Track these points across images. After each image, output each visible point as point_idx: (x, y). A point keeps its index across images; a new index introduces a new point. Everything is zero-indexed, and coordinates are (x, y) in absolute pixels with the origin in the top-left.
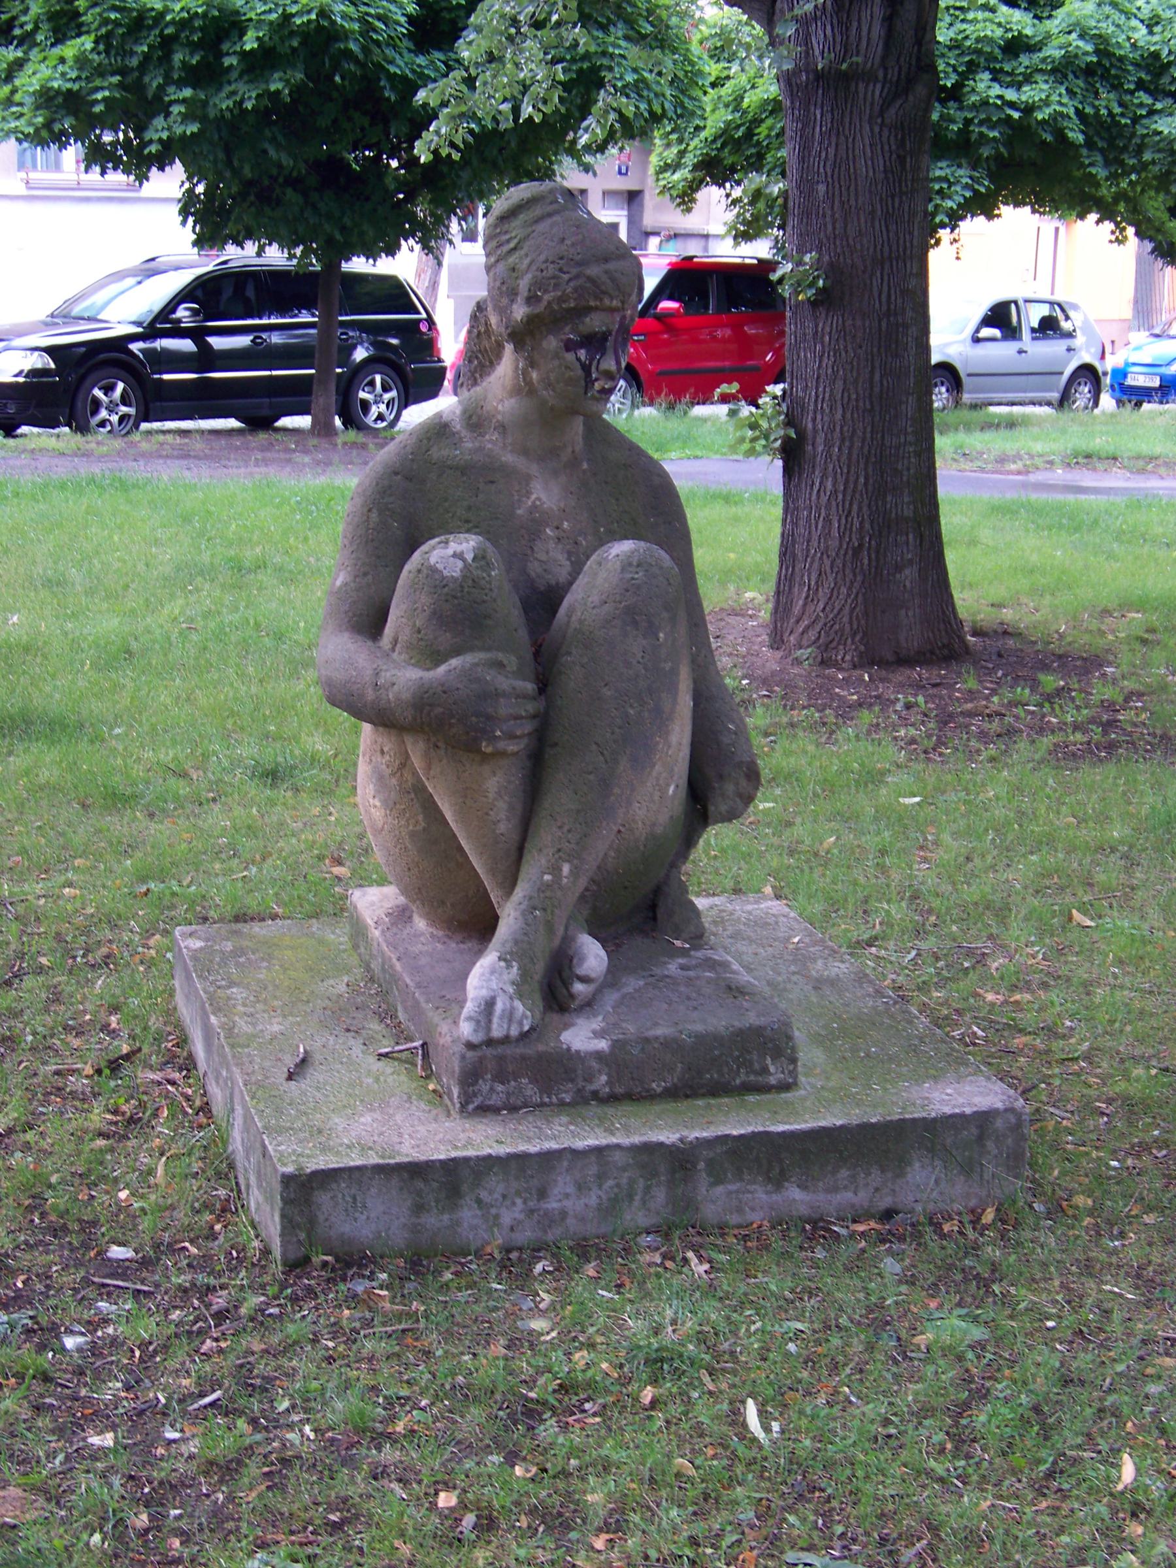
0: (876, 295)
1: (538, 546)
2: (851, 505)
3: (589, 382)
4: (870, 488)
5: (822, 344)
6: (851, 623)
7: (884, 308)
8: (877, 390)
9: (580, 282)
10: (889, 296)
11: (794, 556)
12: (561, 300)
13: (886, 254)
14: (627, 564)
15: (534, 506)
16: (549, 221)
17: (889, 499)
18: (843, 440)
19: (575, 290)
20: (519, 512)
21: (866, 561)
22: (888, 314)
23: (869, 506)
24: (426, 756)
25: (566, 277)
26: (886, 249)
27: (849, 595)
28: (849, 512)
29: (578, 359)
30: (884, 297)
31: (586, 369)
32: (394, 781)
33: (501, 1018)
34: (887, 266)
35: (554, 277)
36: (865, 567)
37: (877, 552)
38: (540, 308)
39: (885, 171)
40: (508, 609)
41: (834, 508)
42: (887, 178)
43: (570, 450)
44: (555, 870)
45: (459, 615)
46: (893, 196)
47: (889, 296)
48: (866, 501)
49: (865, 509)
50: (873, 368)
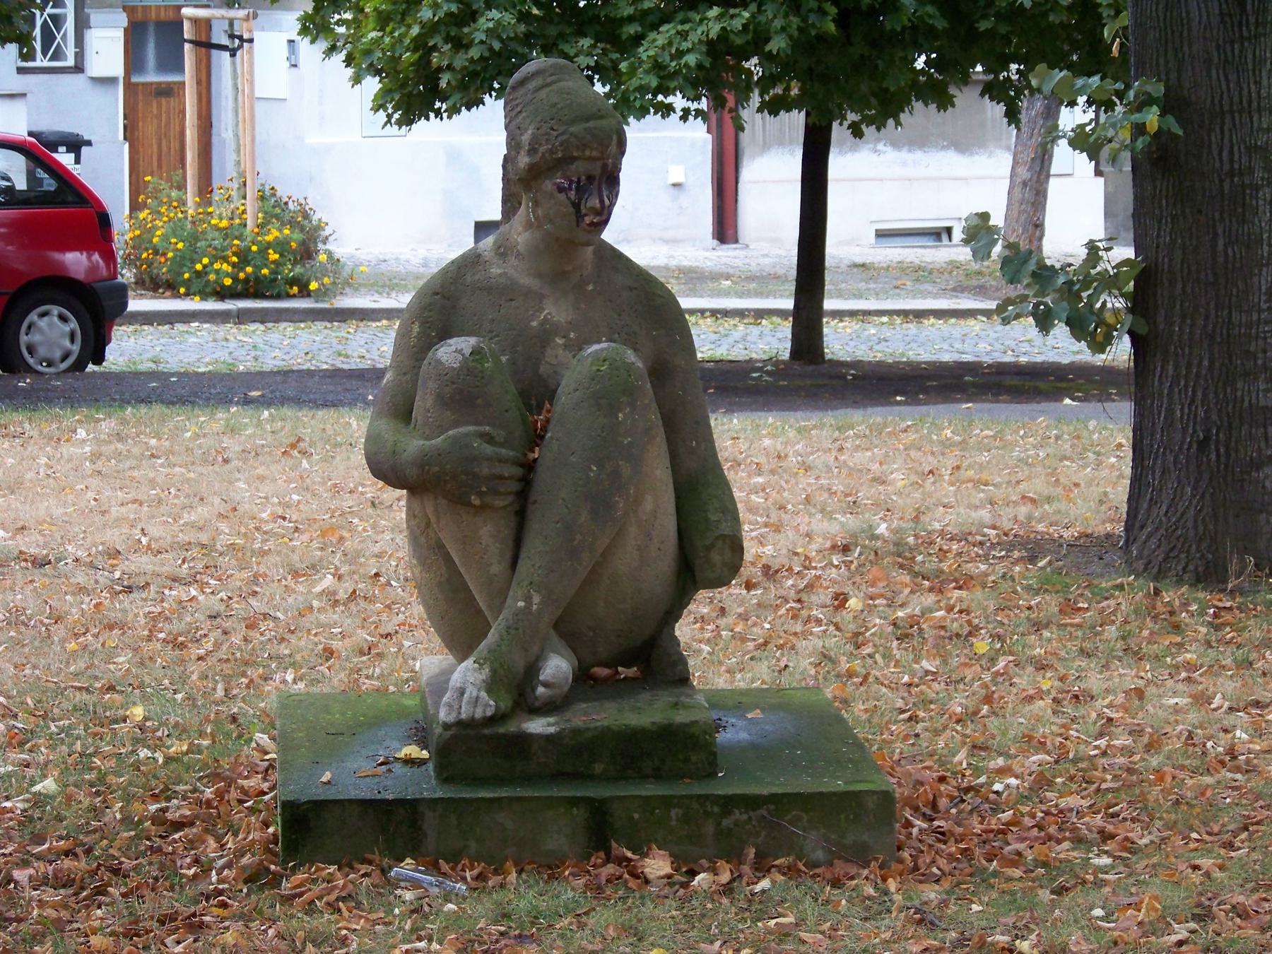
0: (1215, 153)
1: (549, 352)
2: (1194, 391)
3: (579, 216)
4: (1216, 373)
5: (1160, 207)
6: (1195, 527)
7: (1226, 167)
8: (1221, 260)
9: (564, 138)
10: (1231, 152)
11: (1142, 449)
12: (551, 152)
13: (1226, 108)
14: (599, 359)
15: (545, 319)
16: (547, 90)
17: (1240, 385)
18: (1184, 317)
19: (561, 144)
20: (534, 324)
21: (1213, 457)
22: (1231, 174)
23: (1216, 393)
24: (436, 511)
25: (555, 133)
26: (1226, 102)
27: (1193, 496)
28: (1193, 401)
29: (569, 198)
30: (1225, 154)
31: (576, 206)
32: (423, 540)
33: (469, 702)
34: (1228, 120)
35: (546, 134)
36: (1213, 464)
37: (1227, 447)
38: (537, 158)
39: (1221, 14)
40: (505, 394)
41: (1176, 396)
42: (1222, 22)
43: (578, 274)
44: (528, 599)
45: (463, 394)
46: (1232, 42)
47: (1231, 152)
48: (1212, 388)
49: (1211, 396)
50: (1216, 235)
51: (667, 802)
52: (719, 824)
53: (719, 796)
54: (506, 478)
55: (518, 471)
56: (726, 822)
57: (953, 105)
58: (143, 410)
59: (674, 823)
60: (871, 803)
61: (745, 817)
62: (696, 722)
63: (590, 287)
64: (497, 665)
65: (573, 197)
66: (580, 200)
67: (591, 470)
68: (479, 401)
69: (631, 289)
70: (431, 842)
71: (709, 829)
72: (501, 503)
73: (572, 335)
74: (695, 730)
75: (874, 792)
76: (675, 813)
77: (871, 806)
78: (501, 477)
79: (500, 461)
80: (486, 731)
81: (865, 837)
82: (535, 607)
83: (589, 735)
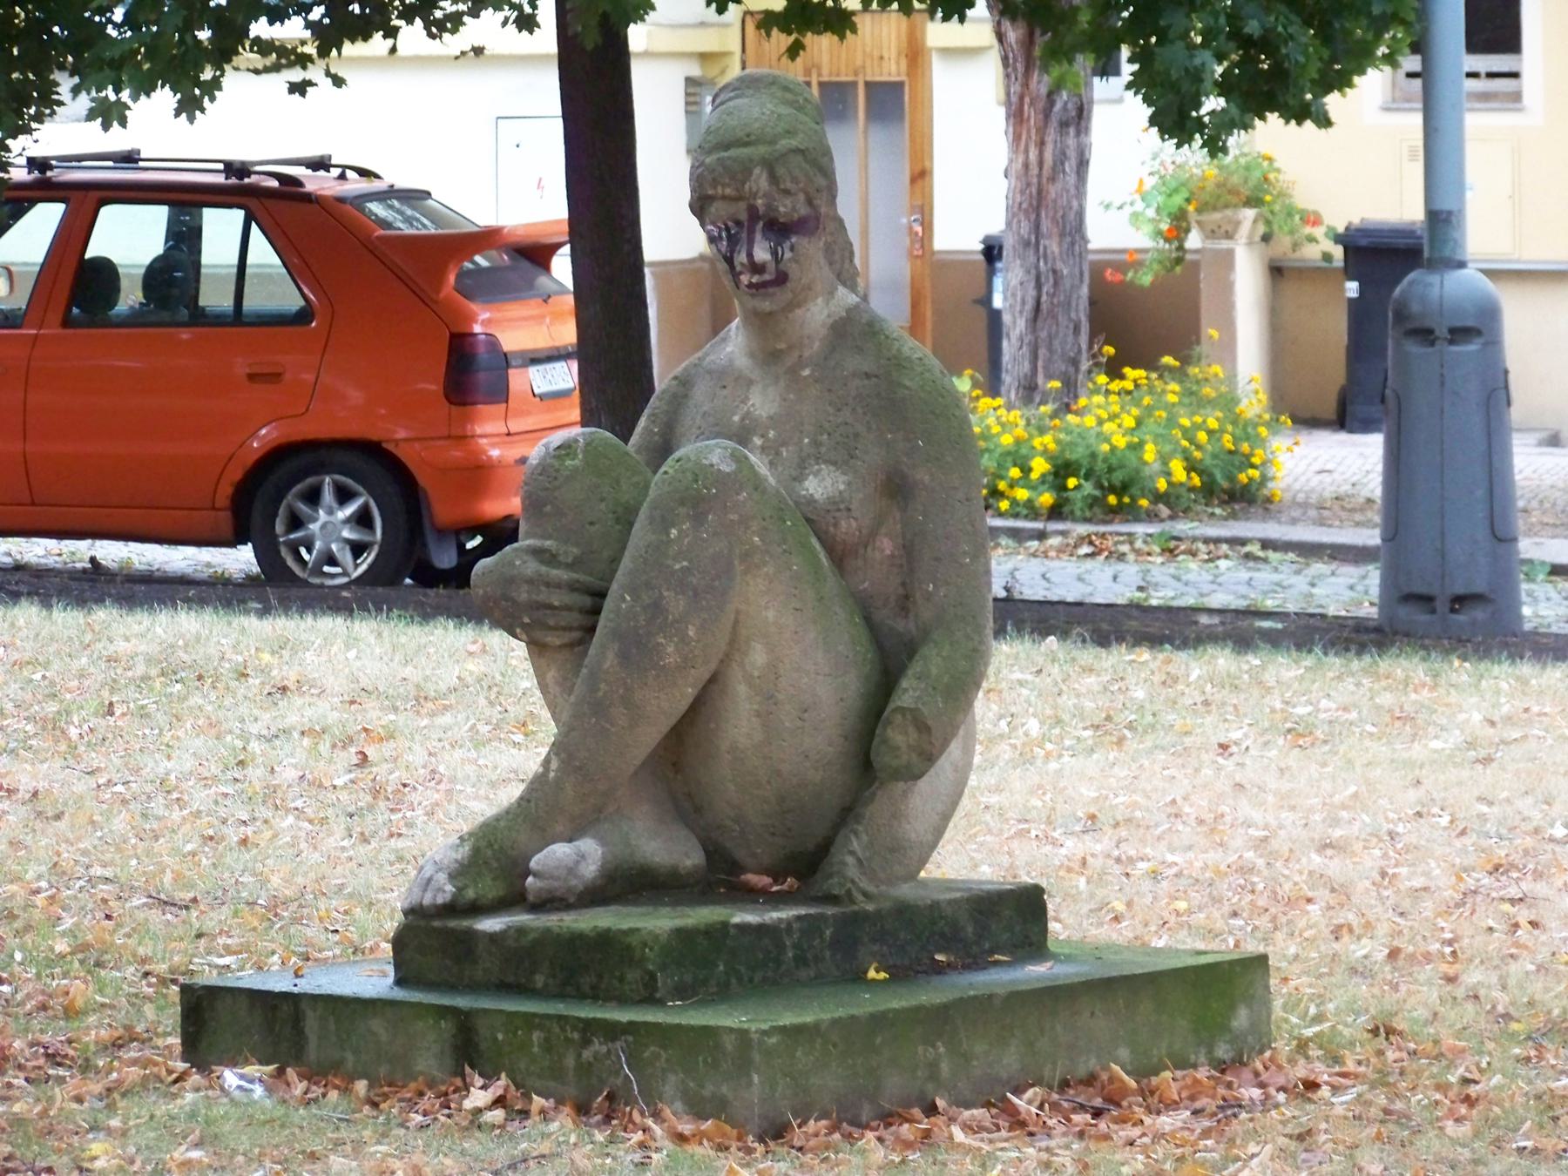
15: (748, 413)
43: (796, 354)
51: (530, 1021)
52: (580, 1055)
53: (579, 1019)
54: (555, 608)
55: (587, 601)
56: (587, 1054)
57: (531, 32)
58: (1144, 655)
59: (536, 1049)
60: (729, 1043)
61: (604, 1049)
62: (638, 930)
63: (806, 372)
64: (483, 844)
65: (723, 249)
66: (732, 252)
67: (624, 600)
68: (548, 508)
69: (868, 376)
70: (312, 1051)
71: (570, 1061)
72: (558, 642)
73: (771, 434)
74: (634, 940)
75: (731, 1030)
76: (536, 1036)
77: (729, 1047)
78: (551, 607)
79: (548, 585)
80: (436, 924)
81: (724, 1089)
82: (552, 774)
83: (532, 936)
